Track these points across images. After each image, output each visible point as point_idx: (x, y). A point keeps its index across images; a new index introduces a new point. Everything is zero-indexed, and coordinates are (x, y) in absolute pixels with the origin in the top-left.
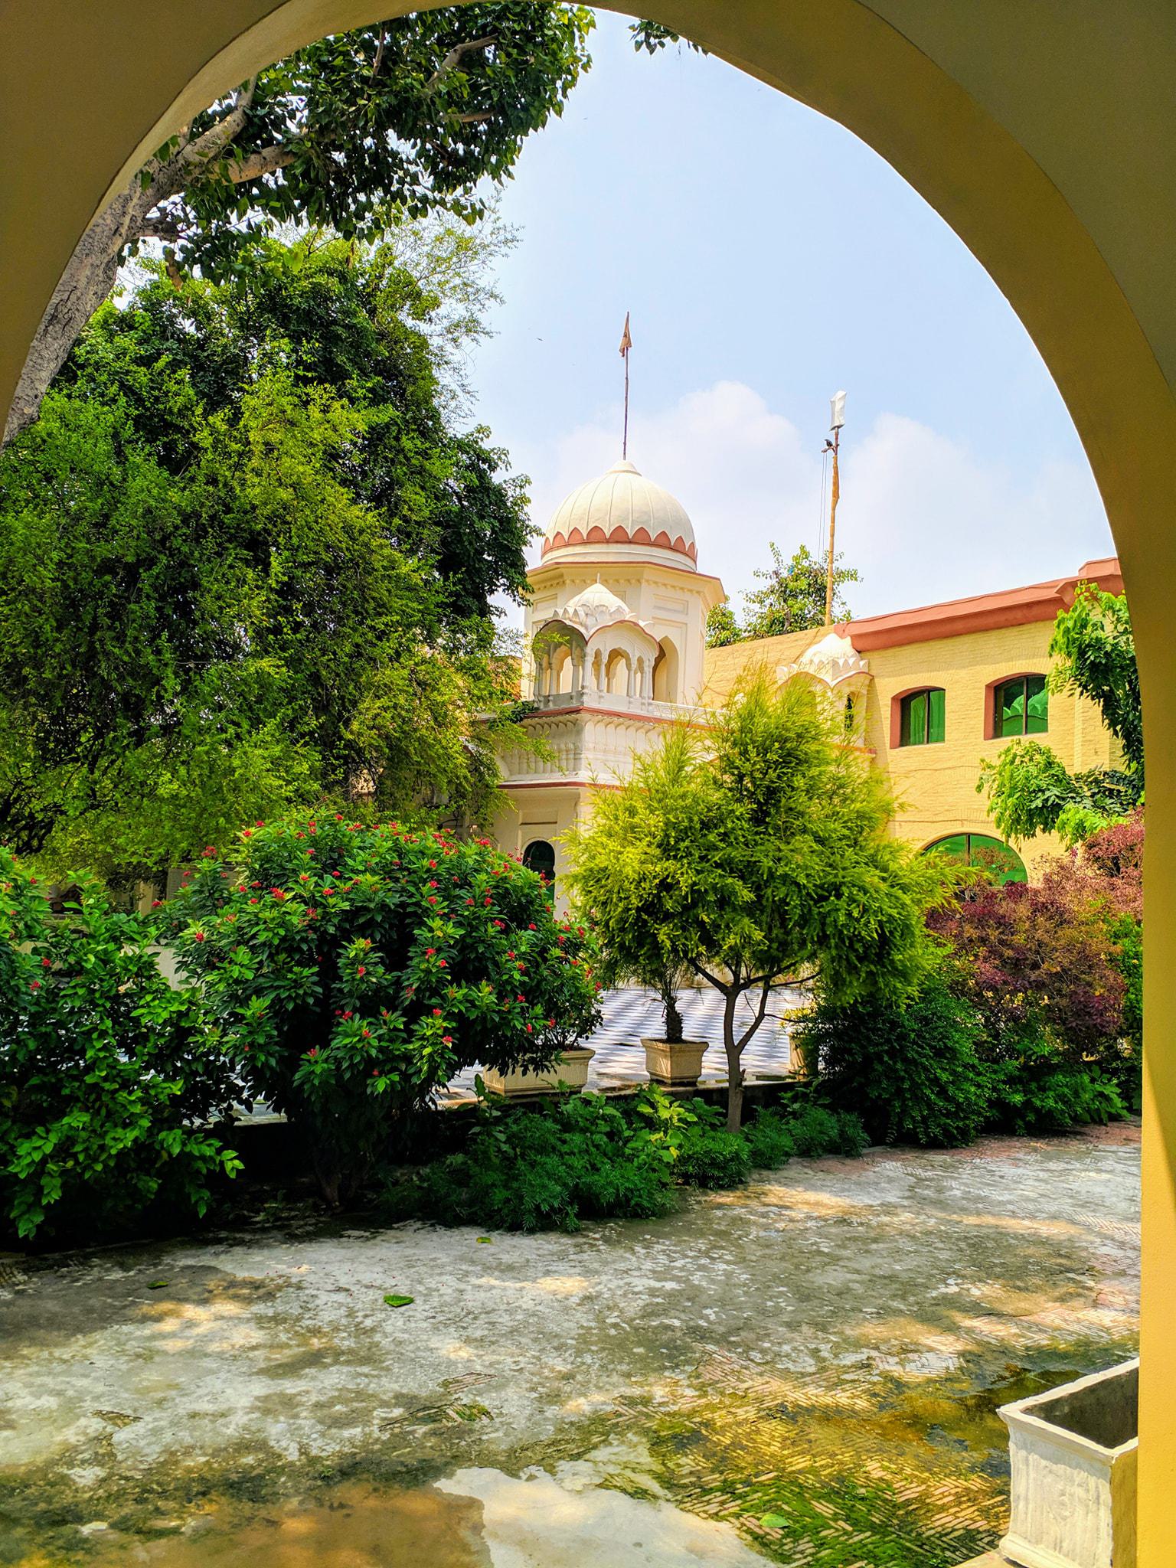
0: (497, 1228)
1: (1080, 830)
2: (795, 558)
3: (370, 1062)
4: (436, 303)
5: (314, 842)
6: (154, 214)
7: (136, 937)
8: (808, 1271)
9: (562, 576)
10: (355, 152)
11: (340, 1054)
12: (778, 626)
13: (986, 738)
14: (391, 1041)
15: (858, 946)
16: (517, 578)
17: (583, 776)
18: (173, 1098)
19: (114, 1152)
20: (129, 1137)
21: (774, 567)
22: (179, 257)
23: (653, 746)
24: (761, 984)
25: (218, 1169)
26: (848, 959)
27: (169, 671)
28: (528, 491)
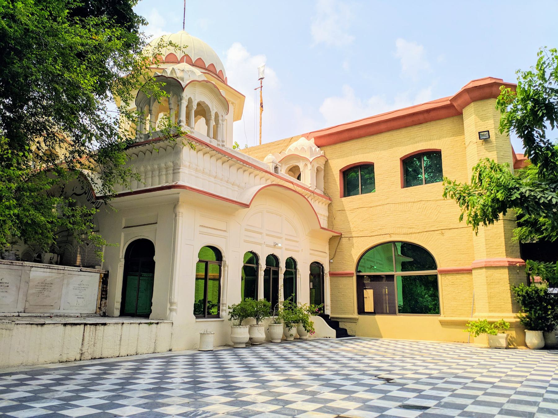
13: (402, 188)
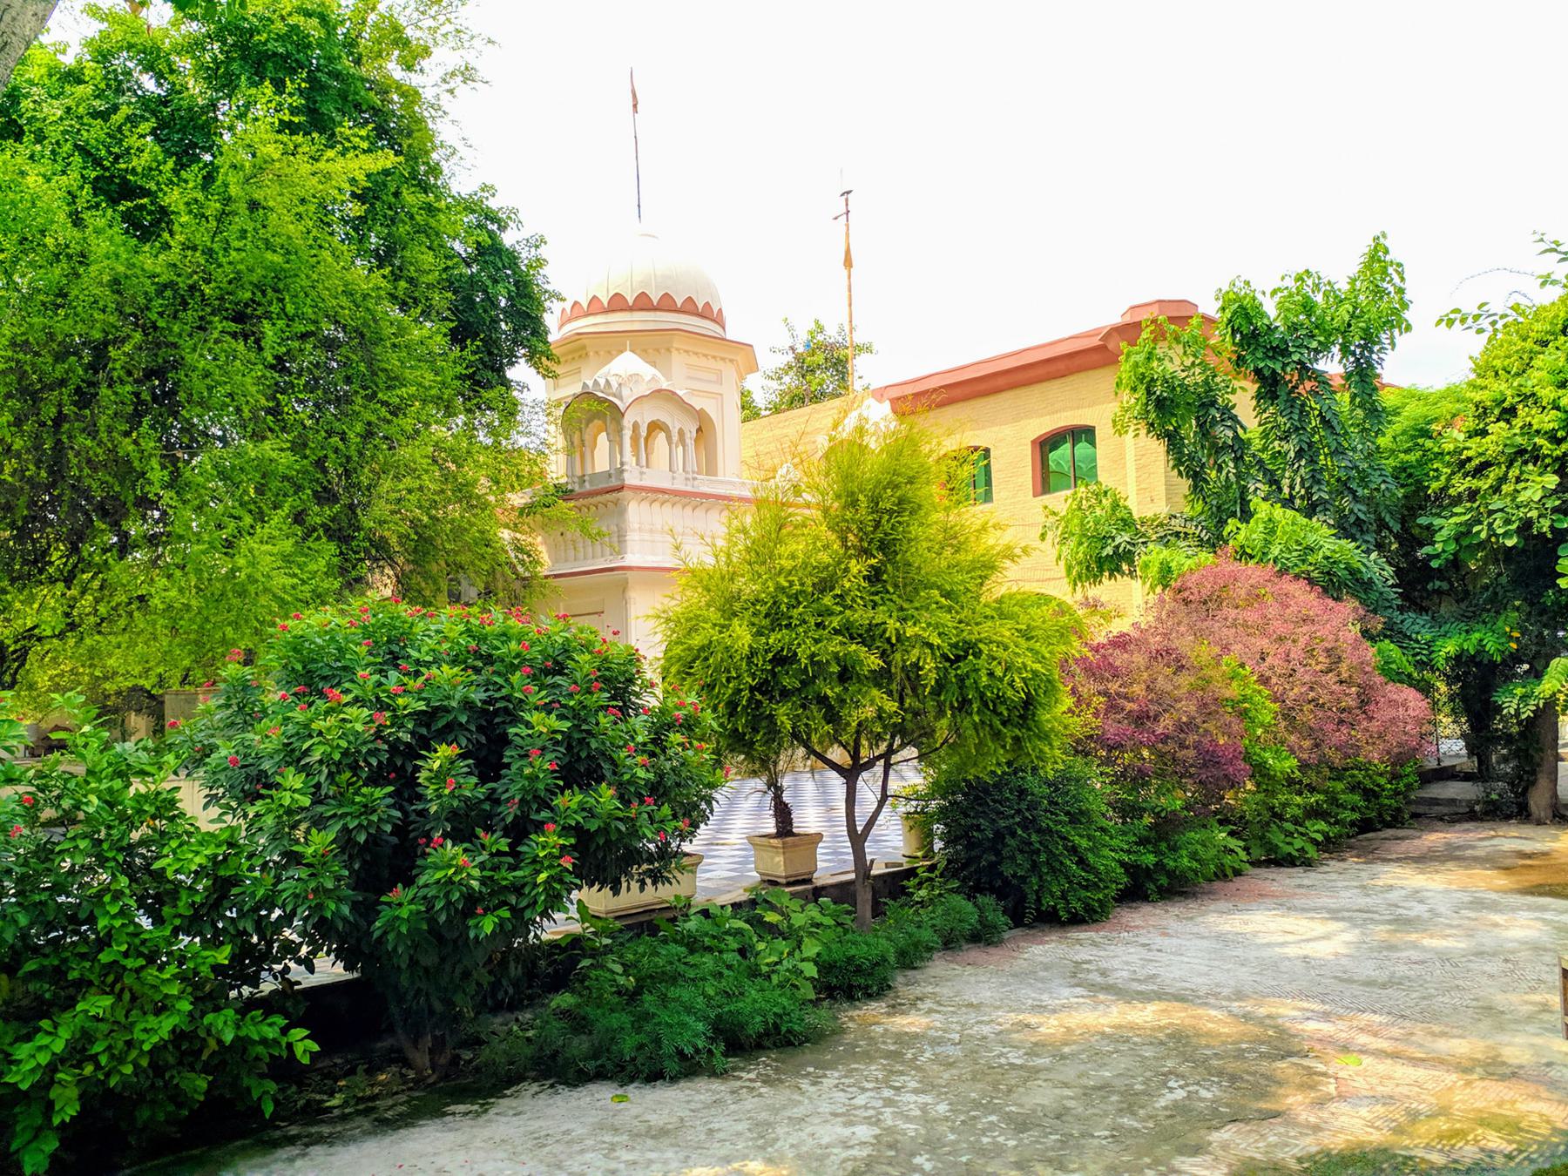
0: (632, 1080)
1: (1166, 571)
2: (811, 332)
3: (472, 900)
4: (426, 52)
5: (367, 633)
7: (148, 769)
8: (1010, 1091)
9: (584, 347)
11: (432, 892)
12: (797, 400)
14: (494, 869)
15: (1003, 709)
17: (631, 559)
18: (216, 968)
19: (146, 1047)
20: (165, 1026)
21: (790, 342)
24: (882, 762)
25: (285, 1054)
26: (991, 726)
27: (155, 463)
28: (544, 252)
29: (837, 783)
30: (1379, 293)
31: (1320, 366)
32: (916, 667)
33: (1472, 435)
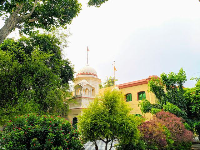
1: (154, 112)
4: (61, 43)
6: (17, 25)
10: (49, 19)
15: (128, 134)
16: (72, 78)
22: (21, 31)
23: (93, 102)
28: (74, 67)
29: (104, 144)
30: (181, 75)
31: (175, 85)
32: (115, 126)
33: (196, 95)
